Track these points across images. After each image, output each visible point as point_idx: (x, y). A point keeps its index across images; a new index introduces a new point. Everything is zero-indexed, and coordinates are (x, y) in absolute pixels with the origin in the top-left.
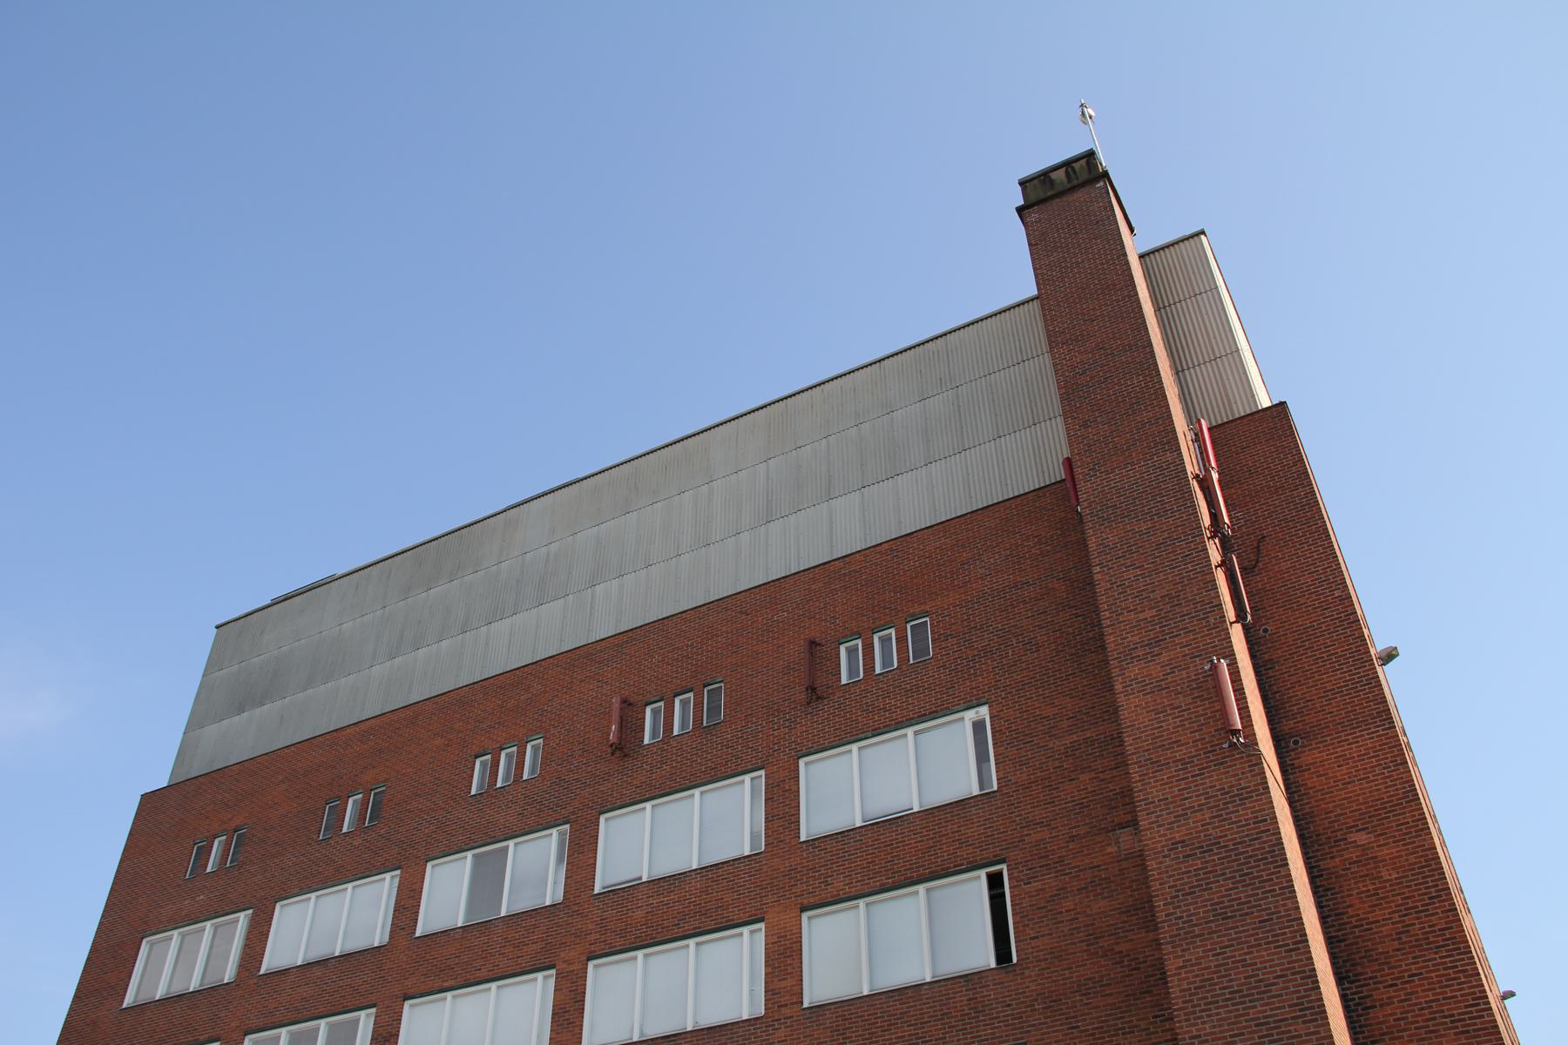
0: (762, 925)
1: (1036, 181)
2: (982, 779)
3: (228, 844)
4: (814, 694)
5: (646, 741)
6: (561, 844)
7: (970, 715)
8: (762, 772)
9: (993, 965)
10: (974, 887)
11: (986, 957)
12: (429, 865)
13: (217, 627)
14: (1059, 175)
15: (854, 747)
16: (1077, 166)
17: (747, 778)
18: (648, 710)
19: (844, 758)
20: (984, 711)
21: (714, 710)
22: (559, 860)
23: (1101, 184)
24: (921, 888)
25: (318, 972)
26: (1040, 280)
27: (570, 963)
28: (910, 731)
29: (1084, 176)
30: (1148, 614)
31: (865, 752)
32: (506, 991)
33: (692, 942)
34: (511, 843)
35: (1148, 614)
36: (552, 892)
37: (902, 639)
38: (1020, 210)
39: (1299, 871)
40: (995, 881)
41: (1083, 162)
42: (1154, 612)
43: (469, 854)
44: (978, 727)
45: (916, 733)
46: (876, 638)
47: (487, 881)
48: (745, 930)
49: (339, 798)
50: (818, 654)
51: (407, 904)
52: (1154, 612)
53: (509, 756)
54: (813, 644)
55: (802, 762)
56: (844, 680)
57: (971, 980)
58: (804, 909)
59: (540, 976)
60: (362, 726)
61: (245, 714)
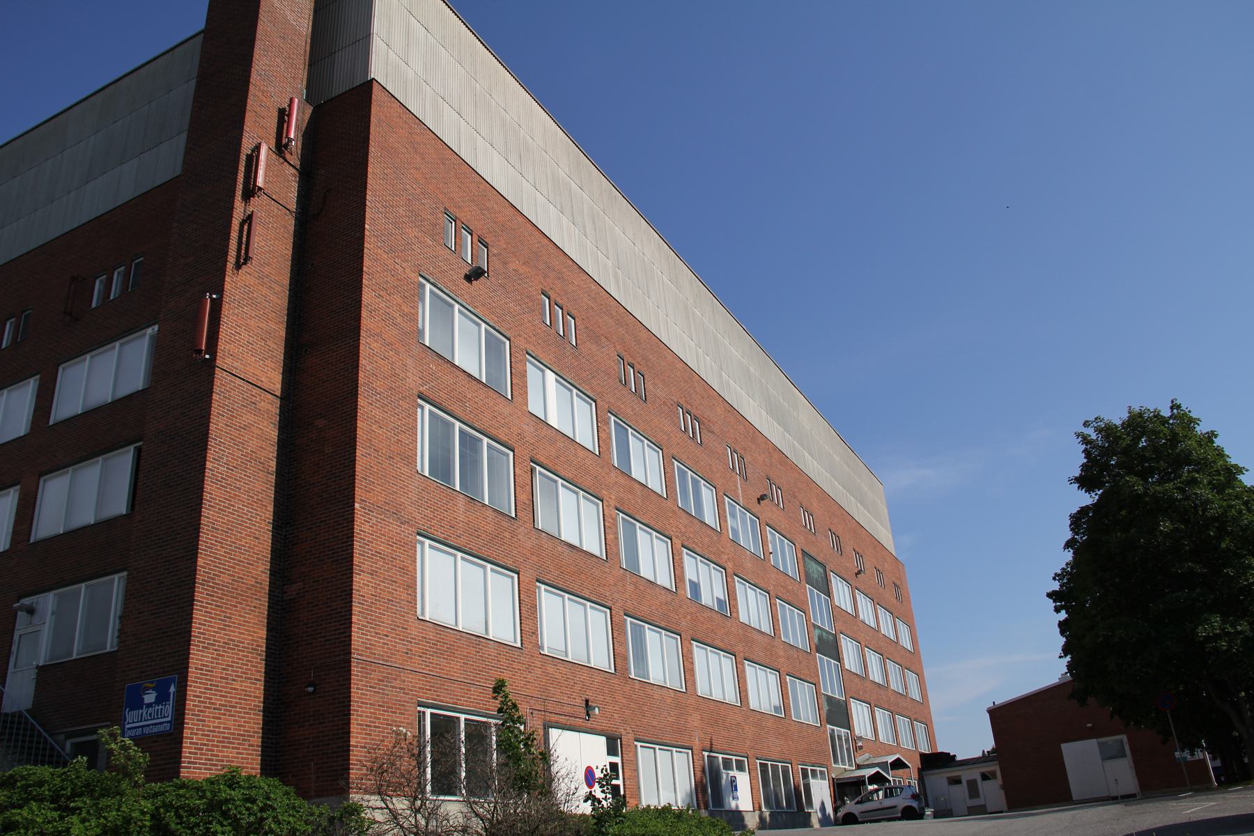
40: (139, 451)
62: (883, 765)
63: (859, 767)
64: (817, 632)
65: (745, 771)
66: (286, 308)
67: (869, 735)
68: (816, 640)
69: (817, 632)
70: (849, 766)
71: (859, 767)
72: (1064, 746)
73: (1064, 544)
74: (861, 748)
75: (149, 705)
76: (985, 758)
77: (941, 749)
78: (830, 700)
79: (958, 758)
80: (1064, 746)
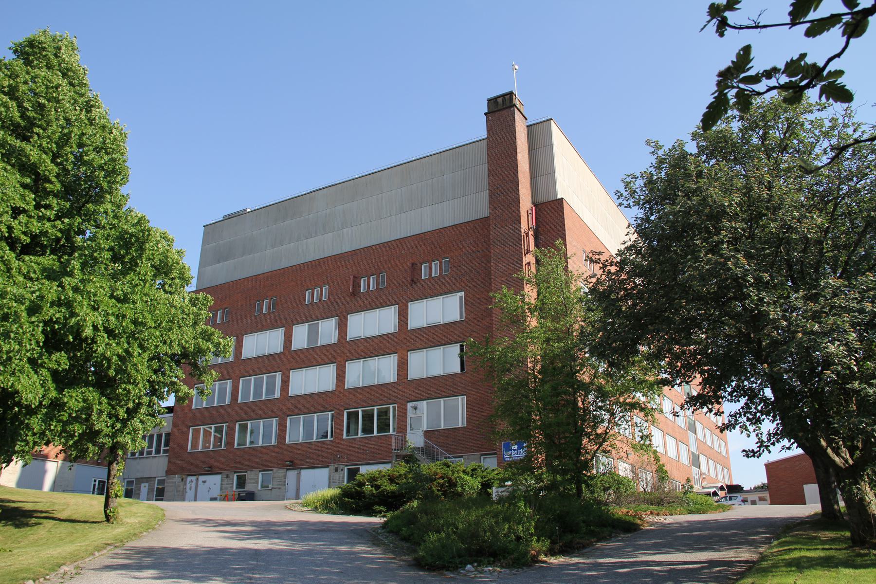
0: (397, 354)
1: (492, 101)
2: (461, 316)
3: (223, 313)
4: (413, 282)
5: (362, 291)
6: (336, 323)
7: (459, 294)
8: (397, 306)
9: (459, 372)
10: (455, 349)
11: (457, 370)
12: (294, 327)
13: (204, 226)
14: (500, 100)
15: (425, 300)
16: (506, 97)
17: (393, 307)
18: (362, 280)
19: (374, 313)
20: (463, 293)
21: (383, 283)
22: (336, 328)
23: (512, 109)
24: (442, 347)
25: (261, 360)
26: (489, 129)
27: (340, 362)
28: (441, 297)
29: (508, 104)
30: (504, 279)
31: (444, 299)
32: (322, 369)
33: (376, 358)
34: (320, 321)
35: (504, 279)
36: (334, 339)
37: (441, 266)
38: (485, 114)
39: (684, 557)
40: (462, 346)
41: (509, 96)
42: (506, 278)
43: (307, 324)
44: (461, 298)
45: (443, 298)
46: (433, 263)
47: (313, 334)
48: (392, 355)
49: (261, 300)
50: (415, 268)
51: (342, 327)
52: (506, 278)
53: (317, 291)
54: (413, 264)
55: (409, 303)
56: (423, 278)
57: (453, 376)
58: (409, 351)
59: (332, 365)
60: (265, 275)
61: (221, 264)
62: (716, 487)
63: (703, 488)
64: (688, 420)
65: (359, 469)
66: (815, 477)
67: (707, 473)
68: (688, 424)
69: (688, 420)
70: (164, 450)
71: (703, 488)
72: (805, 486)
73: (742, 47)
74: (705, 478)
75: (515, 450)
76: (761, 488)
77: (734, 483)
78: (693, 453)
79: (745, 489)
80: (805, 486)
